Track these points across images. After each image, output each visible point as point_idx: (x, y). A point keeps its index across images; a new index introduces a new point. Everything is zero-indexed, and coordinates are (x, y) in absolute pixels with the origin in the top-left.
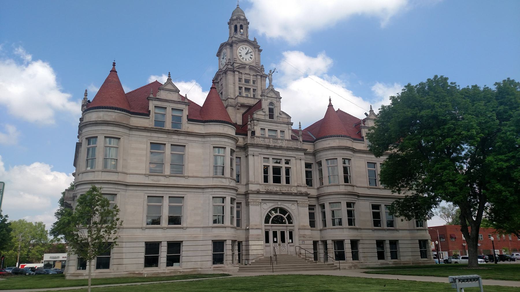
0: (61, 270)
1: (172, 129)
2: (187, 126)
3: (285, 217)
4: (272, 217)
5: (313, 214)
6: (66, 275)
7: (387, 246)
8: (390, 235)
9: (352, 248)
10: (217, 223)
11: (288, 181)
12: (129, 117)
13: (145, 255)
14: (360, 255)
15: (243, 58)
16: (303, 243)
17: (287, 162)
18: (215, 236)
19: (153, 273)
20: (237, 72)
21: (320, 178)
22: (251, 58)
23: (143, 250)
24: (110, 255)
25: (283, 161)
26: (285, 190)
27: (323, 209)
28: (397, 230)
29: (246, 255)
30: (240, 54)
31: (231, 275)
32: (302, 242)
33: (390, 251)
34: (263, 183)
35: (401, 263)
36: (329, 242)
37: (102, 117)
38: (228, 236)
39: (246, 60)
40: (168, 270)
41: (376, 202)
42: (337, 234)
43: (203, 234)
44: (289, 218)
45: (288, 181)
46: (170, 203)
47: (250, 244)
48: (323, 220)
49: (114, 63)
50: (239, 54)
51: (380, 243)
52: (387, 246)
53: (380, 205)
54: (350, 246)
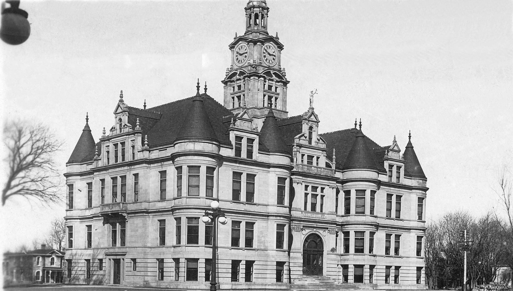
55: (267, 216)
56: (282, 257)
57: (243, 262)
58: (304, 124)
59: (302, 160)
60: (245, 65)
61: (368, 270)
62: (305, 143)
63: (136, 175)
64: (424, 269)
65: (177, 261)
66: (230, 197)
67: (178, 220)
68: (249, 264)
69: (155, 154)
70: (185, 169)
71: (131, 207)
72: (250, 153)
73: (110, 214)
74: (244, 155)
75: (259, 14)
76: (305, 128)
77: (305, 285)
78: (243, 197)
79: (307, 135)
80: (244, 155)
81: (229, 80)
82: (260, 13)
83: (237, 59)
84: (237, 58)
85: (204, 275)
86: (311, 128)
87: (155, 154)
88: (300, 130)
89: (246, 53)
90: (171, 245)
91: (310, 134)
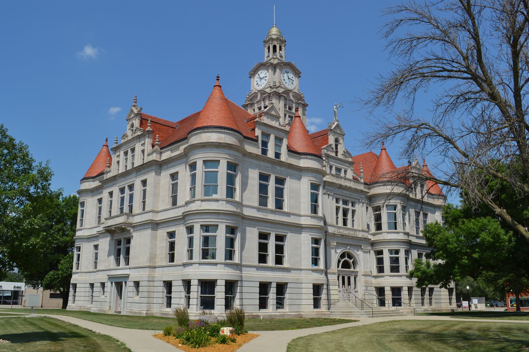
5: (382, 258)
6: (190, 315)
7: (273, 291)
9: (227, 292)
13: (201, 294)
14: (286, 302)
18: (316, 280)
21: (191, 188)
24: (214, 294)
27: (191, 233)
29: (240, 299)
33: (314, 298)
34: (343, 226)
35: (436, 310)
36: (194, 283)
37: (224, 139)
40: (279, 312)
41: (265, 230)
42: (190, 272)
43: (364, 281)
44: (354, 263)
48: (377, 267)
51: (264, 288)
52: (273, 291)
53: (400, 250)
54: (223, 289)
55: (298, 228)
56: (320, 278)
57: (274, 285)
58: (330, 135)
59: (260, 244)
60: (266, 87)
61: (407, 293)
62: (333, 154)
63: (144, 183)
64: (454, 290)
65: (187, 284)
66: (256, 204)
67: (190, 230)
68: (281, 288)
69: (167, 155)
70: (200, 164)
71: (136, 220)
72: (278, 155)
73: (113, 229)
74: (271, 154)
75: (277, 46)
76: (331, 140)
77: (436, 340)
78: (271, 204)
79: (334, 146)
80: (271, 154)
81: (249, 102)
82: (278, 44)
83: (257, 84)
84: (257, 83)
85: (223, 302)
86: (337, 140)
87: (167, 155)
88: (326, 140)
89: (266, 77)
90: (181, 263)
91: (336, 146)
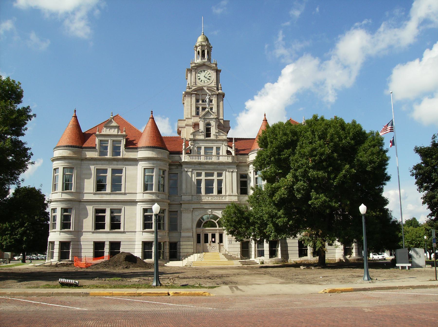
0: (281, 259)
1: (99, 157)
2: (124, 154)
3: (216, 222)
4: (204, 222)
8: (92, 237)
10: (107, 227)
11: (220, 192)
12: (81, 151)
15: (201, 81)
16: (230, 243)
17: (220, 175)
19: (96, 264)
20: (194, 95)
22: (199, 79)
23: (92, 247)
25: (216, 173)
26: (216, 200)
28: (124, 232)
30: (199, 78)
31: (421, 267)
32: (230, 242)
38: (146, 238)
39: (204, 82)
45: (220, 192)
46: (96, 213)
47: (181, 244)
49: (75, 110)
50: (210, 76)
